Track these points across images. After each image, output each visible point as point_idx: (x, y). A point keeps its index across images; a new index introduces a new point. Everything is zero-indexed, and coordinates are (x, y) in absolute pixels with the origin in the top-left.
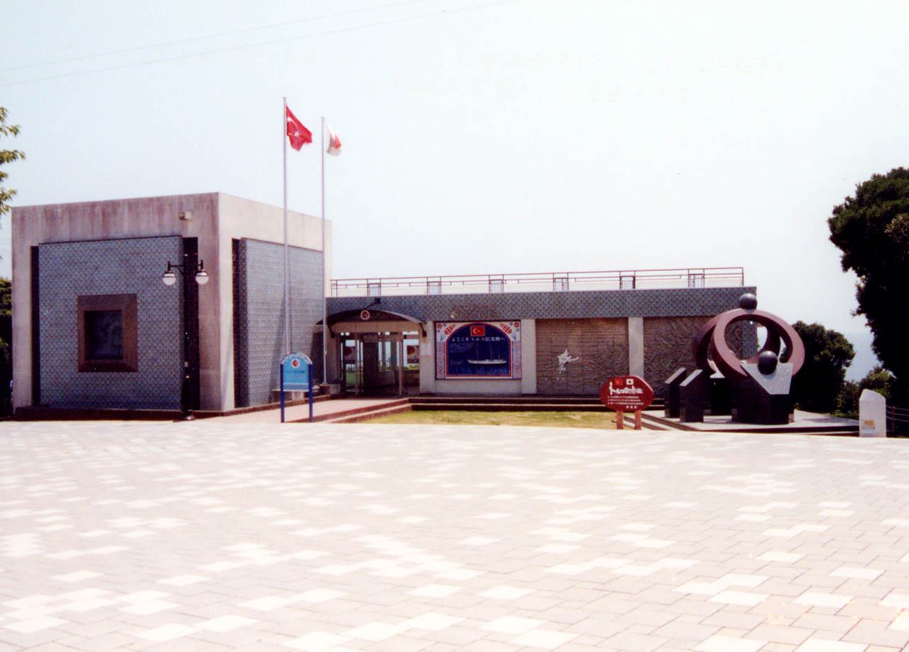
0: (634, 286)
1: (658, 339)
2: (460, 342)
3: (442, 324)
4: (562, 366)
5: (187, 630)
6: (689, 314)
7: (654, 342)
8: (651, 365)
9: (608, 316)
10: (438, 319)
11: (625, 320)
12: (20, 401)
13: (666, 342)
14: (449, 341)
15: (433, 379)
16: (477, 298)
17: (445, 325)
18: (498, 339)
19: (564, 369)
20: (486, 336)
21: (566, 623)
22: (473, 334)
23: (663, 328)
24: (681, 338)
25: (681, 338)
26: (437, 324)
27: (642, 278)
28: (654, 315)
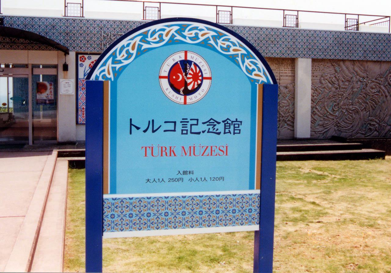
0: (389, 32)
1: (323, 82)
3: (86, 56)
6: (353, 58)
7: (320, 85)
8: (322, 91)
9: (333, 57)
10: (80, 51)
11: (292, 61)
13: (330, 85)
17: (89, 58)
21: (354, 25)
23: (329, 71)
24: (343, 81)
25: (343, 81)
26: (80, 56)
28: (322, 57)
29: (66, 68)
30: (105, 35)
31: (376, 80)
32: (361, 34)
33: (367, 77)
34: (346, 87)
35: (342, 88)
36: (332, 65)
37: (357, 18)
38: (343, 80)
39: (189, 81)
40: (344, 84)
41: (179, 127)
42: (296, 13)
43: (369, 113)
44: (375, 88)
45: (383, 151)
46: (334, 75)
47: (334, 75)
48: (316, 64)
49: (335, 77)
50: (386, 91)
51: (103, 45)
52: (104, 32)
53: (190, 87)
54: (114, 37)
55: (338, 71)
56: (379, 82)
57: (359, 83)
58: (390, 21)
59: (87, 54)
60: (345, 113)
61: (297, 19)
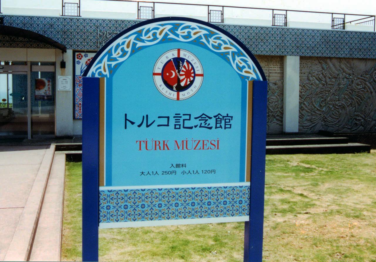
1: (311, 78)
3: (83, 54)
6: (339, 56)
9: (320, 55)
10: (77, 49)
11: (281, 59)
12: (320, 184)
13: (317, 82)
15: (232, 125)
16: (328, 35)
17: (86, 56)
23: (316, 68)
24: (329, 78)
25: (329, 78)
26: (77, 54)
29: (63, 65)
30: (101, 34)
31: (362, 77)
32: (347, 32)
35: (329, 84)
38: (330, 77)
40: (331, 81)
42: (284, 12)
43: (355, 109)
44: (360, 85)
47: (321, 72)
48: (304, 61)
50: (371, 87)
52: (100, 31)
53: (183, 84)
54: (110, 36)
55: (325, 68)
56: (364, 79)
57: (345, 80)
58: (375, 20)
59: (83, 52)
60: (332, 108)
61: (286, 18)
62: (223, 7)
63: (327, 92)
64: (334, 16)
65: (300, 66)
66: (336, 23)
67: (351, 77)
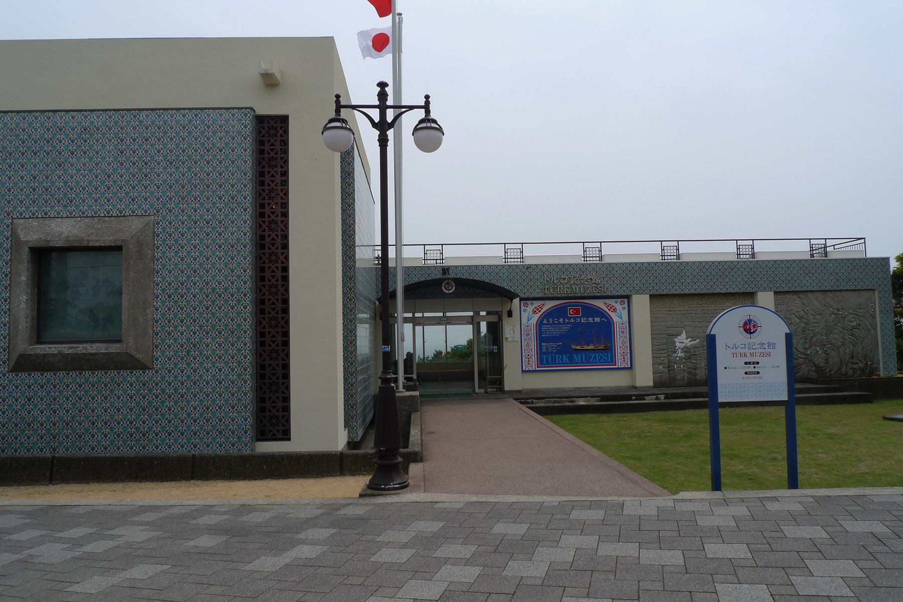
2: (553, 323)
3: (529, 302)
4: (680, 351)
5: (15, 557)
6: (823, 288)
14: (540, 323)
17: (532, 304)
18: (597, 320)
19: (683, 355)
20: (583, 316)
22: (570, 314)
24: (813, 315)
25: (813, 315)
27: (391, 240)
29: (510, 314)
30: (549, 280)
31: (854, 311)
32: (830, 260)
33: (843, 309)
34: (817, 321)
35: (812, 323)
36: (799, 297)
37: (824, 243)
38: (814, 313)
39: (751, 328)
40: (814, 319)
41: (747, 347)
42: (751, 242)
43: (849, 350)
44: (854, 321)
45: (866, 393)
46: (802, 308)
47: (802, 308)
48: (779, 297)
49: (803, 310)
50: (868, 323)
51: (546, 289)
52: (547, 276)
53: (752, 331)
54: (557, 281)
55: (807, 304)
56: (858, 314)
57: (833, 316)
58: (865, 243)
60: (818, 351)
61: (753, 248)
62: (522, 244)
63: (811, 332)
64: (739, 243)
65: (775, 303)
66: (509, 255)
67: (840, 313)
